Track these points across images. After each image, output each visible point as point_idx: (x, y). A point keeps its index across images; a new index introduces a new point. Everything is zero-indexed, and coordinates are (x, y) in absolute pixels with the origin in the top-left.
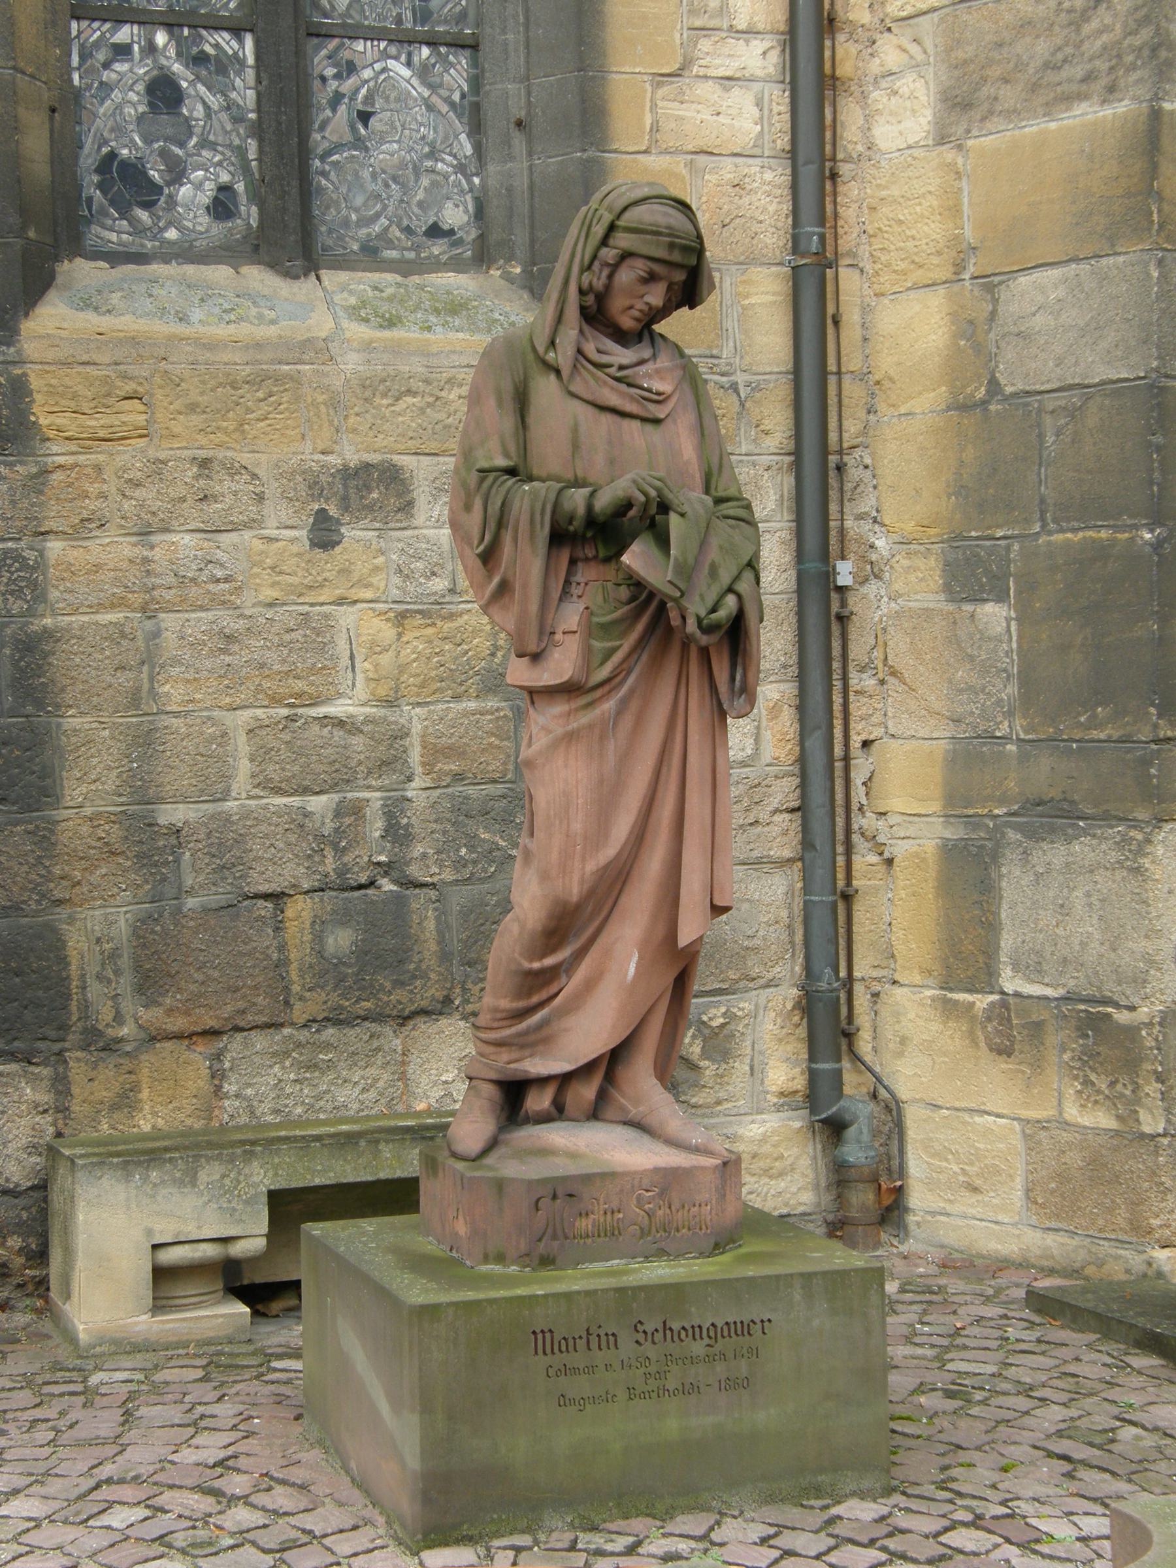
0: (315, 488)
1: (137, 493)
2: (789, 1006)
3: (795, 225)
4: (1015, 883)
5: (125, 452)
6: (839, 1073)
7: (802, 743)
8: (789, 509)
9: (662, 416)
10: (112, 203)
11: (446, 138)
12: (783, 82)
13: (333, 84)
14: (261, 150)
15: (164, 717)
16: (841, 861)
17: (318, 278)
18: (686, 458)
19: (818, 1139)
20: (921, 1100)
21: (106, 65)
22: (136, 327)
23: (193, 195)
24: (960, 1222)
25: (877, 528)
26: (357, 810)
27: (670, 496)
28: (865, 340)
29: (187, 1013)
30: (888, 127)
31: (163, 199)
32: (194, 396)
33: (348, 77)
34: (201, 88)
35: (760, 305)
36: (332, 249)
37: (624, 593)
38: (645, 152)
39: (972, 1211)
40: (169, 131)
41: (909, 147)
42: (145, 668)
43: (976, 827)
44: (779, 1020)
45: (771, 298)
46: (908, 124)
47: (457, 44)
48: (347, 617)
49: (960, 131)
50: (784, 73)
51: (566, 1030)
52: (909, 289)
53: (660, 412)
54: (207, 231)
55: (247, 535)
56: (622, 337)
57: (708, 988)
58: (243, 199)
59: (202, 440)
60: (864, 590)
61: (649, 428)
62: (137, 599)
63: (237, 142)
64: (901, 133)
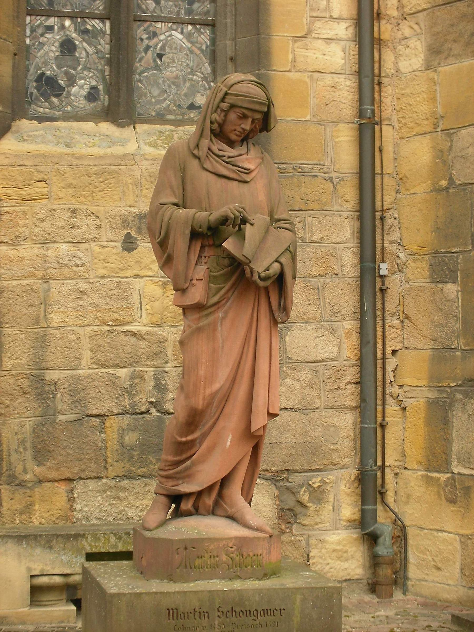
0: (125, 223)
1: (42, 225)
2: (353, 478)
3: (361, 105)
4: (459, 418)
5: (36, 206)
6: (376, 510)
7: (361, 351)
8: (357, 237)
9: (249, 180)
10: (42, 95)
11: (198, 65)
12: (355, 41)
13: (146, 42)
14: (111, 71)
15: (50, 329)
16: (379, 408)
17: (135, 128)
18: (260, 199)
19: (365, 544)
20: (416, 525)
21: (42, 35)
22: (45, 149)
23: (79, 91)
24: (431, 585)
25: (400, 248)
26: (141, 377)
27: (246, 215)
28: (395, 159)
29: (58, 470)
30: (405, 62)
31: (65, 93)
32: (71, 181)
33: (153, 38)
34: (85, 44)
35: (344, 141)
36: (142, 115)
37: (226, 262)
38: (289, 71)
39: (437, 579)
40: (69, 63)
41: (414, 71)
42: (43, 306)
43: (442, 392)
44: (347, 485)
45: (349, 138)
46: (414, 60)
47: (205, 24)
48: (138, 284)
49: (436, 63)
50: (356, 37)
51: (198, 471)
52: (414, 135)
53: (247, 178)
54: (84, 107)
55: (93, 244)
56: (231, 144)
57: (313, 468)
58: (102, 92)
59: (74, 201)
60: (393, 277)
61: (241, 185)
62: (39, 274)
63: (100, 67)
64: (410, 65)
